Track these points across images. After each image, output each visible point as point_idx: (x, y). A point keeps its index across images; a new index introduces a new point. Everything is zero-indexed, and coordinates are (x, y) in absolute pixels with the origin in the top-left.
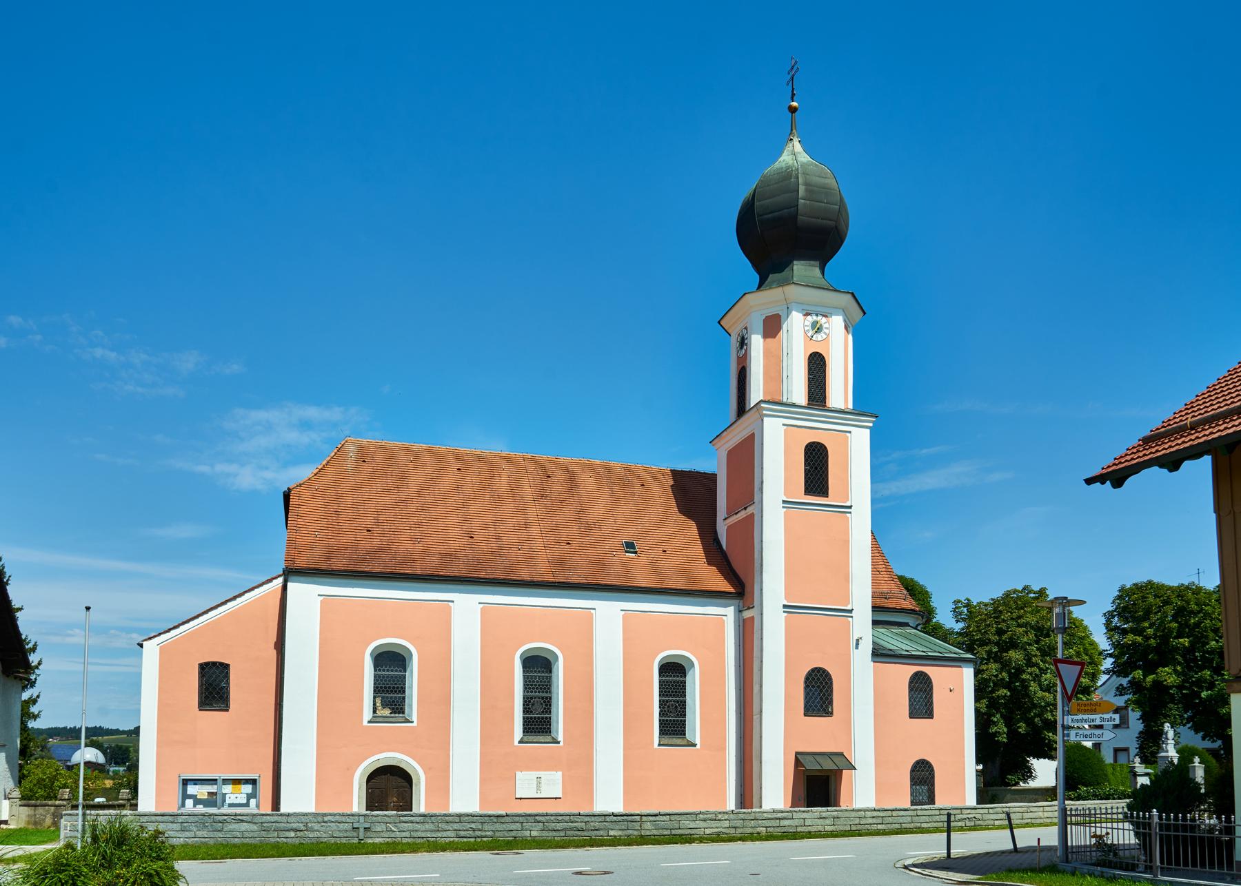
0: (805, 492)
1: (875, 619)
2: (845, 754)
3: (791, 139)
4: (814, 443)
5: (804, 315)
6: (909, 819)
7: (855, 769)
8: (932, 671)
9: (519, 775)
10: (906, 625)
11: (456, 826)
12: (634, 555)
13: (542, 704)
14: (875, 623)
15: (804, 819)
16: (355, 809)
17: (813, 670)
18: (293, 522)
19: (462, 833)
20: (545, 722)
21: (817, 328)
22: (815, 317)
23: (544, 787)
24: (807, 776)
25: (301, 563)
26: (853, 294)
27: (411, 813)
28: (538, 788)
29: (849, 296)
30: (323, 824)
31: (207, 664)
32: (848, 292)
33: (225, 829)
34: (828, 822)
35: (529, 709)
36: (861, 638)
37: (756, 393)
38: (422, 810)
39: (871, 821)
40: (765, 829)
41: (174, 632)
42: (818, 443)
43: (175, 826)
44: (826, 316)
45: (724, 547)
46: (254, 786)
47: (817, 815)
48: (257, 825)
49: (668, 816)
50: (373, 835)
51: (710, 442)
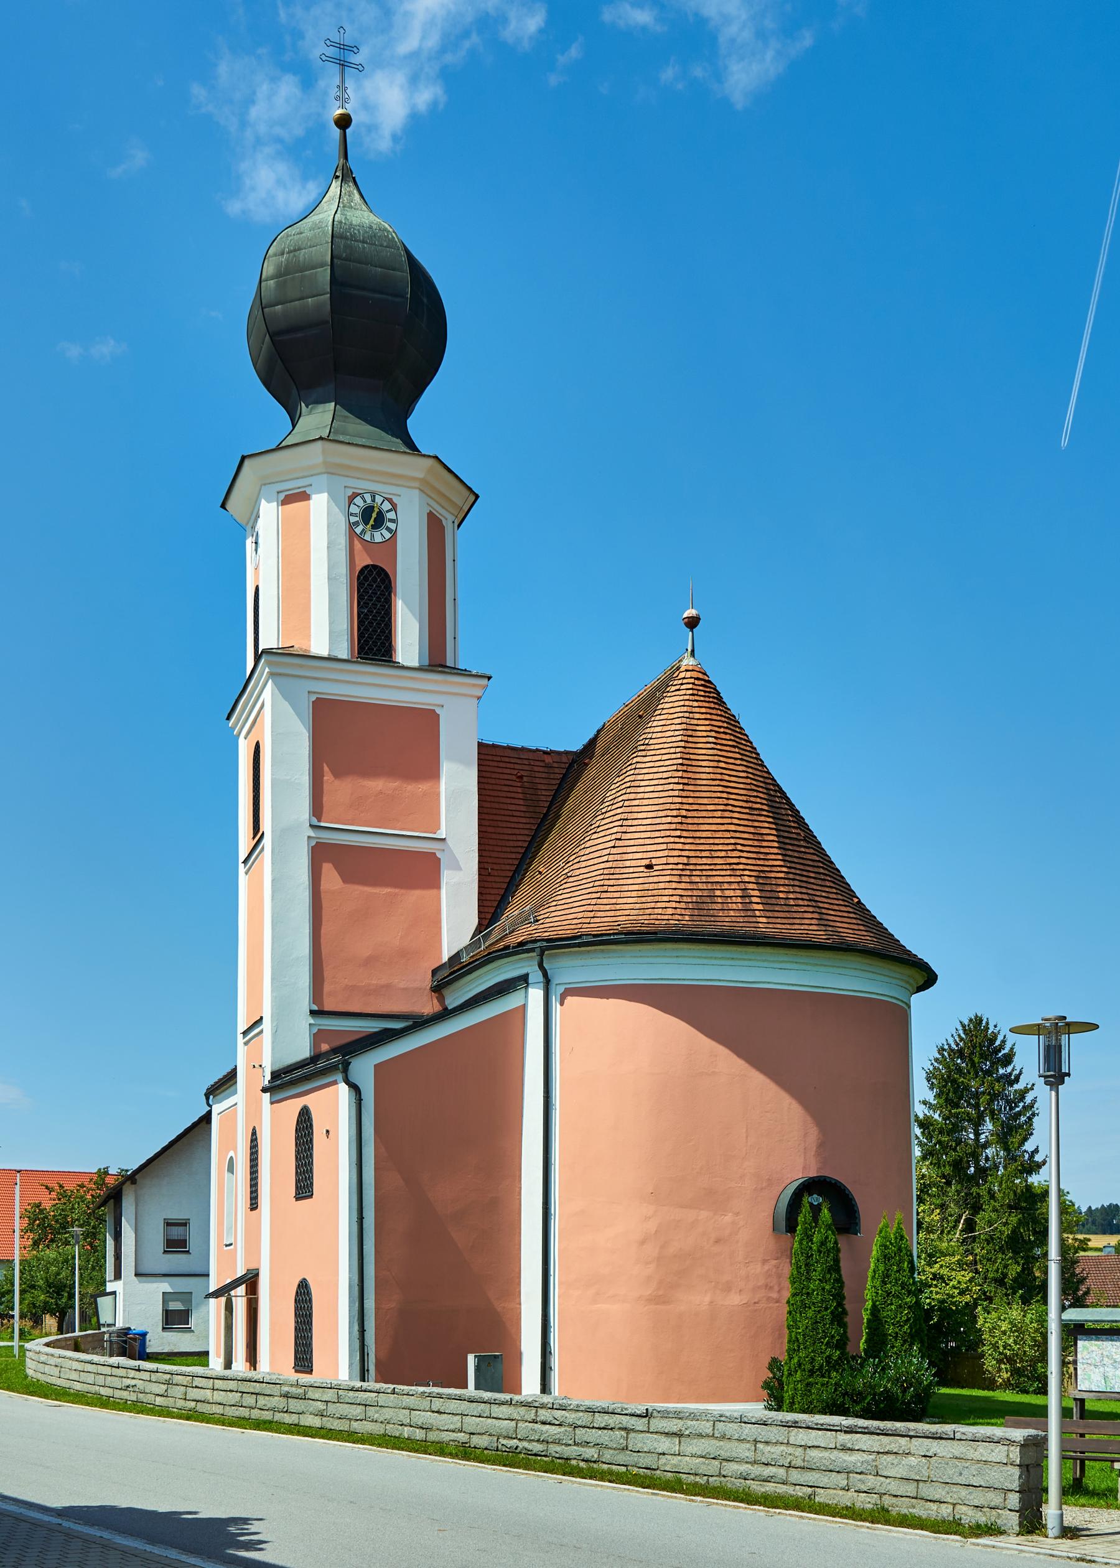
7: (1090, 1207)
26: (436, 458)
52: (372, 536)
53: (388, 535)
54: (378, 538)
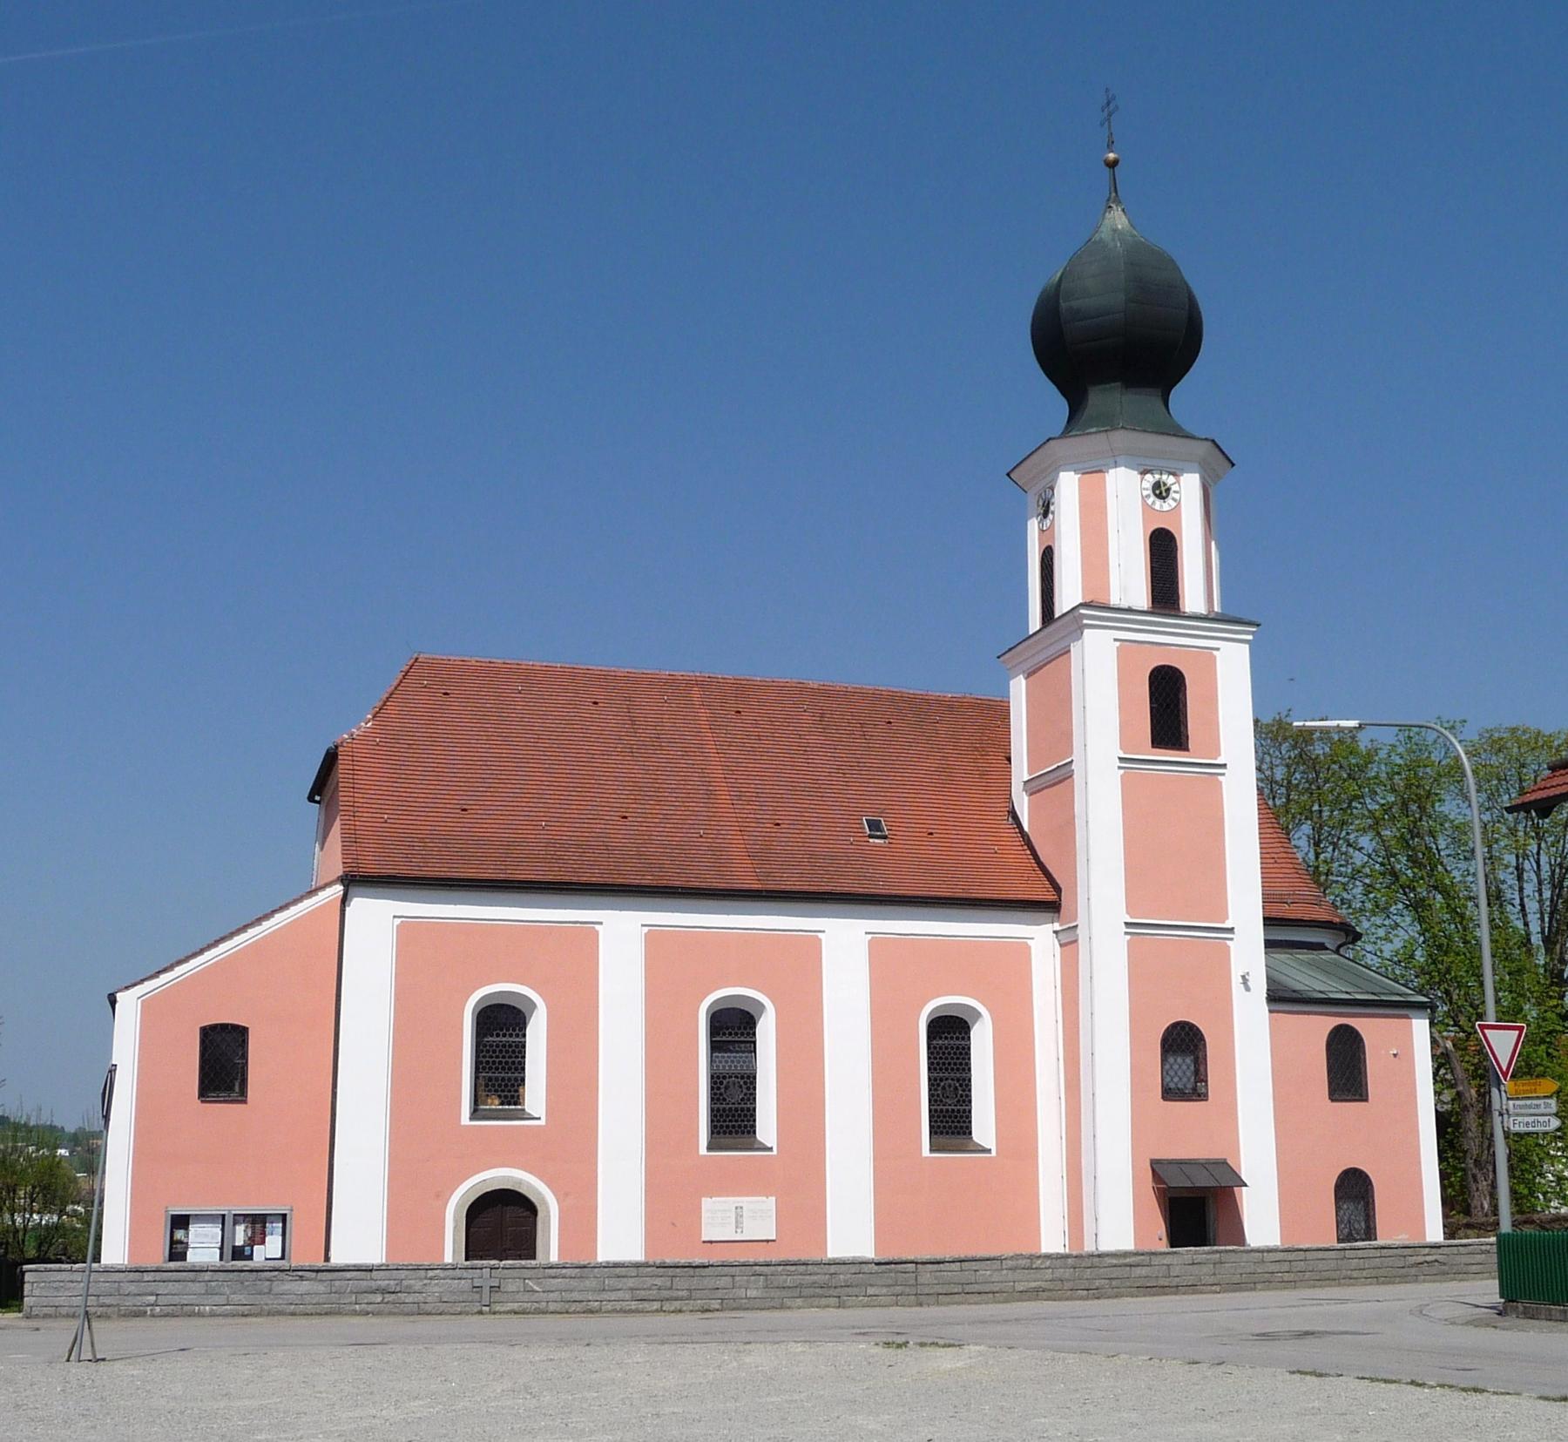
0: (1153, 743)
1: (1268, 938)
2: (1229, 1162)
3: (1110, 207)
4: (1163, 667)
5: (1141, 473)
6: (1333, 1264)
7: (1246, 1185)
8: (1366, 1026)
9: (707, 1203)
10: (1321, 947)
11: (631, 1283)
12: (882, 841)
13: (741, 1087)
14: (1269, 944)
15: (1168, 1265)
16: (448, 1258)
17: (1175, 1025)
18: (346, 799)
19: (642, 1294)
20: (745, 1116)
21: (1161, 491)
22: (1157, 476)
23: (746, 1222)
24: (1170, 1199)
25: (372, 867)
26: (1213, 441)
27: (533, 1262)
28: (738, 1224)
29: (1210, 443)
30: (425, 1281)
31: (214, 1027)
32: (1206, 439)
33: (275, 1290)
34: (1205, 1269)
35: (721, 1094)
36: (1248, 973)
37: (1068, 596)
38: (554, 1258)
39: (1273, 1268)
40: (1107, 1281)
41: (165, 978)
42: (1169, 667)
43: (197, 1287)
44: (1174, 474)
45: (1026, 828)
46: (268, 1218)
47: (1188, 1259)
48: (325, 1284)
49: (959, 1264)
50: (504, 1297)
51: (999, 657)
52: (1161, 506)
53: (1174, 504)
54: (1166, 507)
